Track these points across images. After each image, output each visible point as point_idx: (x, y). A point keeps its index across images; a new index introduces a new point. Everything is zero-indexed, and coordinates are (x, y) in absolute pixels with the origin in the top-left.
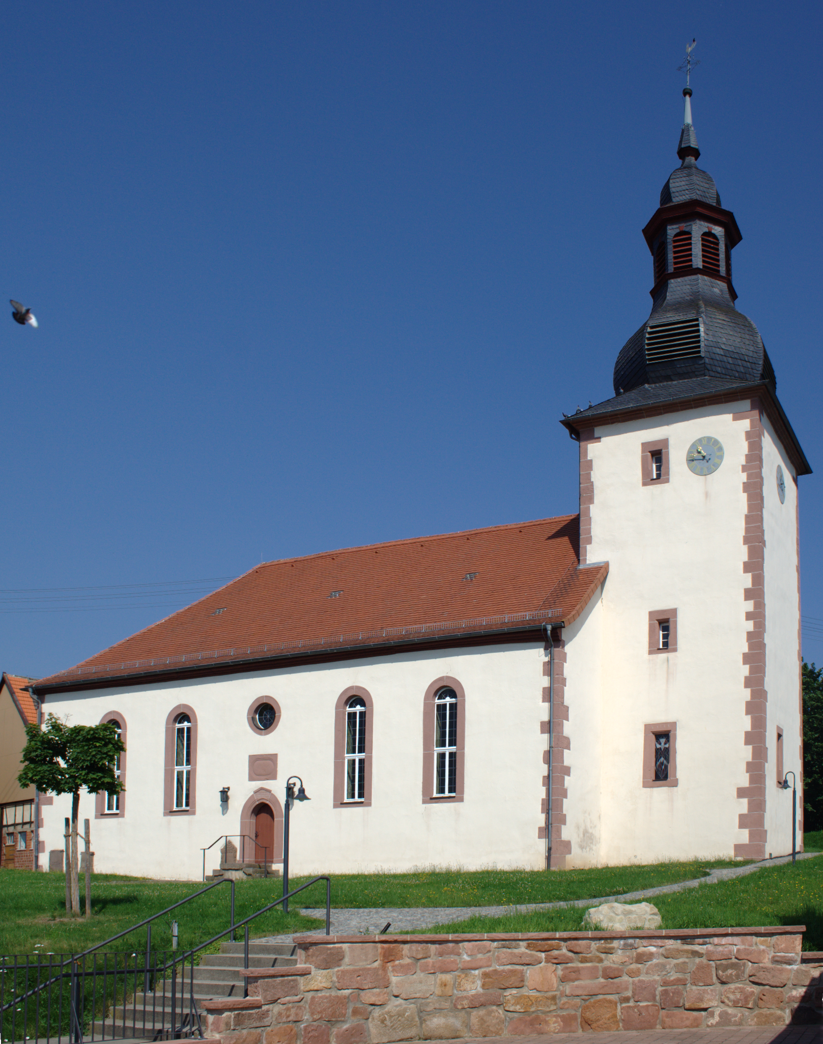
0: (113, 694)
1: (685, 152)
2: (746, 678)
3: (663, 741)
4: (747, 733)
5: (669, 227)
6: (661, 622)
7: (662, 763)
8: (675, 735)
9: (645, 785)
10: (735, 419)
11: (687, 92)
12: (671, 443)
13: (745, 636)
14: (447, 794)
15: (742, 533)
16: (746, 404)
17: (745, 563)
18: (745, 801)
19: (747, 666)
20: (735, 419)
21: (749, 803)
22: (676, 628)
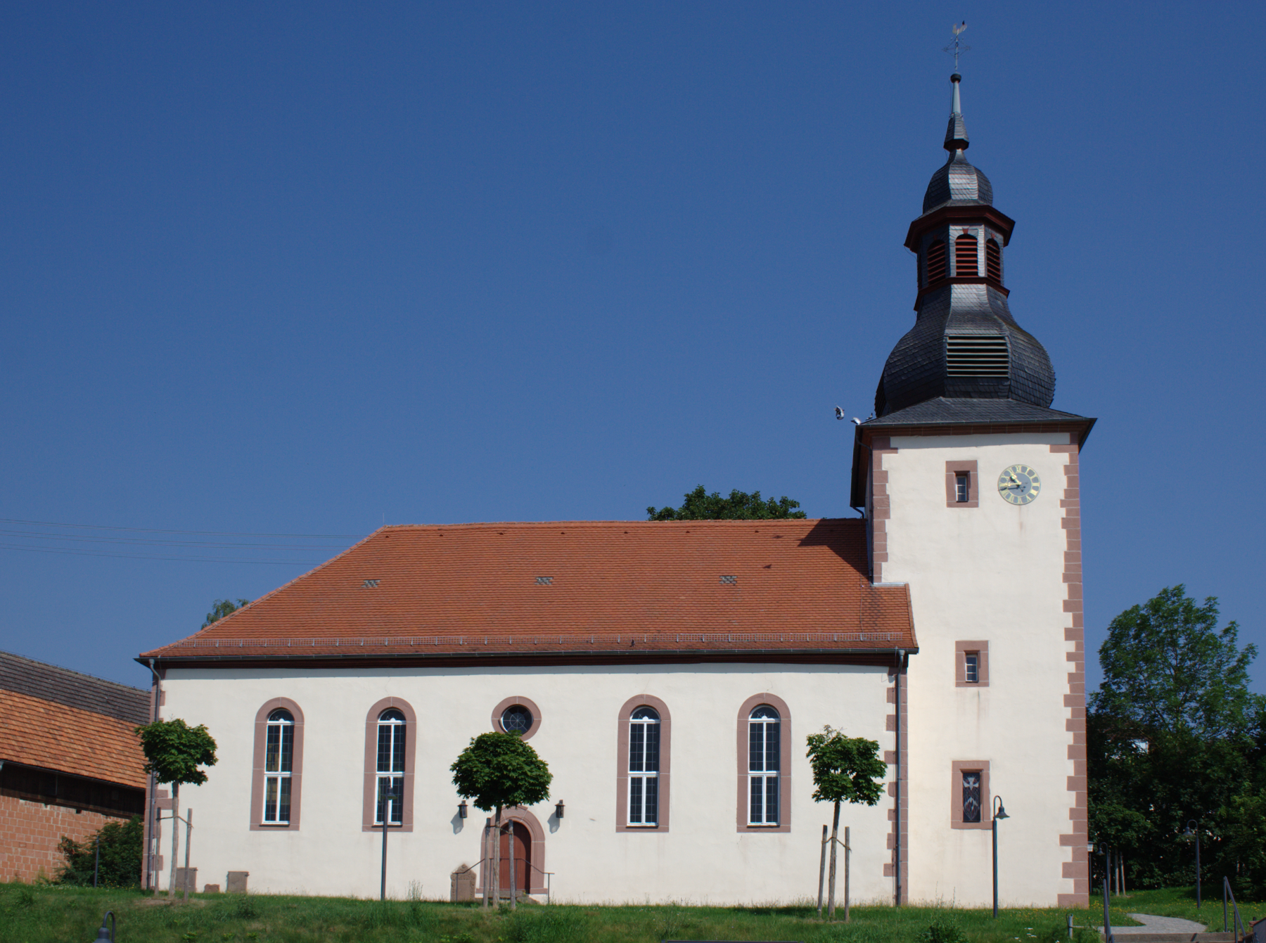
0: (281, 677)
1: (952, 144)
2: (1068, 721)
3: (971, 780)
4: (1070, 778)
5: (952, 227)
6: (968, 653)
7: (971, 804)
8: (988, 775)
9: (954, 826)
10: (1052, 451)
11: (955, 78)
12: (980, 465)
13: (1066, 678)
14: (764, 823)
15: (1061, 570)
16: (1066, 437)
17: (1065, 602)
18: (1069, 849)
19: (1069, 709)
20: (1052, 451)
21: (1074, 852)
22: (987, 661)
